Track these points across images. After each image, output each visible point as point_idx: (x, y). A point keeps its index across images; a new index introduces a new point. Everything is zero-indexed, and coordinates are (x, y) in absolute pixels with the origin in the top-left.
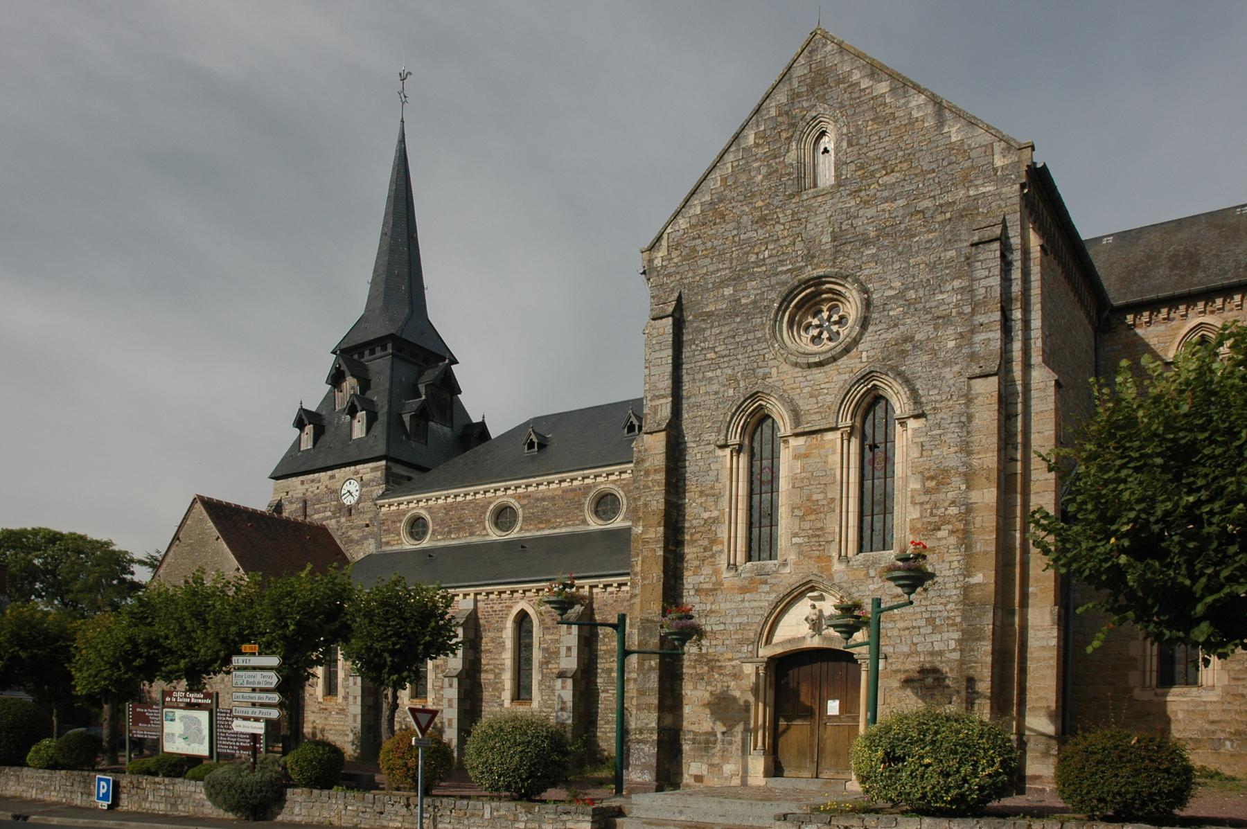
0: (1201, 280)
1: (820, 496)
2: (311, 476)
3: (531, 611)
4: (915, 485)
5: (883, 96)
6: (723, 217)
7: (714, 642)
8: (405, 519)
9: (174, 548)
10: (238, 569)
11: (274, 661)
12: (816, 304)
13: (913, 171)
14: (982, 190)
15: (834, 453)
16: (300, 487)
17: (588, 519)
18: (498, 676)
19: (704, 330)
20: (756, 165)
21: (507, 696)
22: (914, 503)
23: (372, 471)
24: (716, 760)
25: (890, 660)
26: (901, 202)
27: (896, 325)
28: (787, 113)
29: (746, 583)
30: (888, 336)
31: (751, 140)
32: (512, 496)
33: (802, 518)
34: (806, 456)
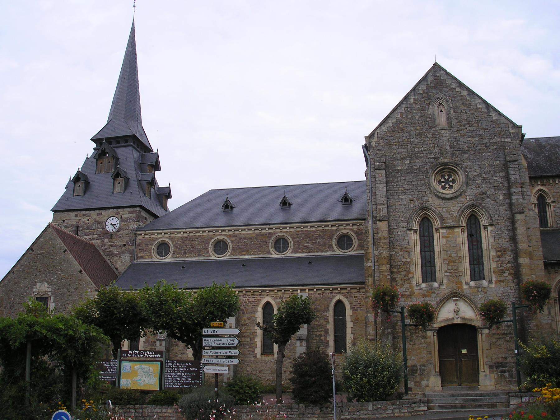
1: (455, 255)
2: (83, 212)
3: (273, 302)
4: (493, 253)
5: (465, 96)
6: (402, 130)
9: (28, 255)
10: (81, 271)
12: (443, 172)
13: (479, 127)
14: (506, 140)
15: (459, 237)
16: (74, 218)
17: (271, 251)
18: (253, 339)
19: (398, 177)
21: (258, 350)
22: (494, 261)
24: (418, 379)
26: (477, 139)
28: (427, 93)
29: (425, 292)
30: (476, 191)
31: (412, 101)
32: (226, 235)
33: (448, 264)
34: (447, 237)
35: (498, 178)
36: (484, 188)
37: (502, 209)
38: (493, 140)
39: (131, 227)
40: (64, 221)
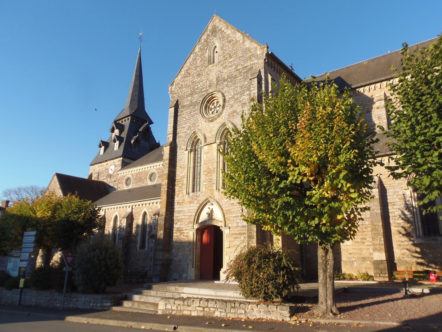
0: (122, 113)
7: (182, 223)
8: (125, 178)
14: (254, 62)
20: (198, 58)
23: (118, 161)
25: (231, 229)
26: (234, 67)
27: (232, 107)
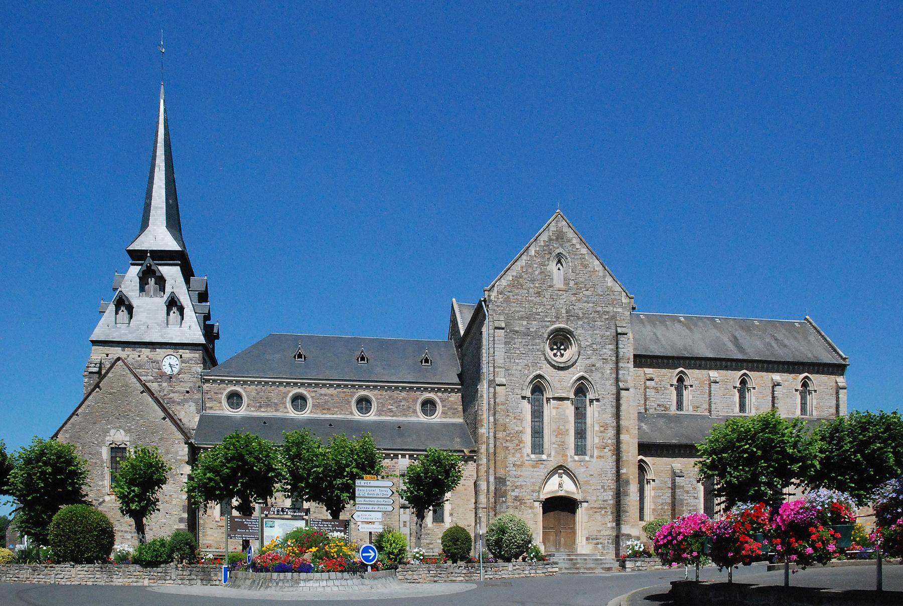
4: (597, 428)
6: (522, 286)
9: (94, 394)
11: (723, 499)
35: (608, 350)
36: (594, 359)
37: (608, 383)
38: (607, 309)
39: (193, 370)
40: (107, 355)
